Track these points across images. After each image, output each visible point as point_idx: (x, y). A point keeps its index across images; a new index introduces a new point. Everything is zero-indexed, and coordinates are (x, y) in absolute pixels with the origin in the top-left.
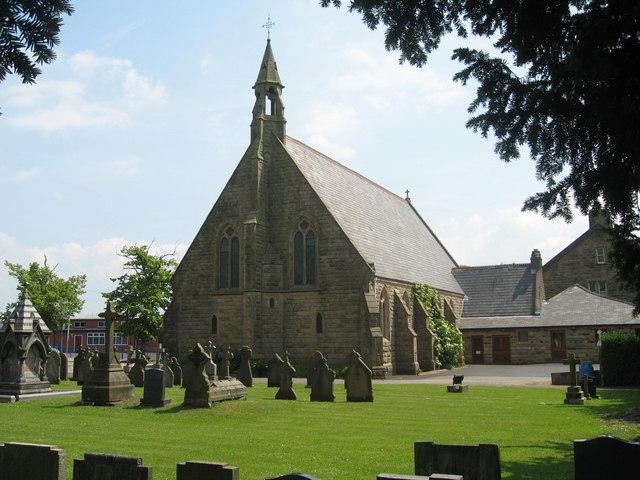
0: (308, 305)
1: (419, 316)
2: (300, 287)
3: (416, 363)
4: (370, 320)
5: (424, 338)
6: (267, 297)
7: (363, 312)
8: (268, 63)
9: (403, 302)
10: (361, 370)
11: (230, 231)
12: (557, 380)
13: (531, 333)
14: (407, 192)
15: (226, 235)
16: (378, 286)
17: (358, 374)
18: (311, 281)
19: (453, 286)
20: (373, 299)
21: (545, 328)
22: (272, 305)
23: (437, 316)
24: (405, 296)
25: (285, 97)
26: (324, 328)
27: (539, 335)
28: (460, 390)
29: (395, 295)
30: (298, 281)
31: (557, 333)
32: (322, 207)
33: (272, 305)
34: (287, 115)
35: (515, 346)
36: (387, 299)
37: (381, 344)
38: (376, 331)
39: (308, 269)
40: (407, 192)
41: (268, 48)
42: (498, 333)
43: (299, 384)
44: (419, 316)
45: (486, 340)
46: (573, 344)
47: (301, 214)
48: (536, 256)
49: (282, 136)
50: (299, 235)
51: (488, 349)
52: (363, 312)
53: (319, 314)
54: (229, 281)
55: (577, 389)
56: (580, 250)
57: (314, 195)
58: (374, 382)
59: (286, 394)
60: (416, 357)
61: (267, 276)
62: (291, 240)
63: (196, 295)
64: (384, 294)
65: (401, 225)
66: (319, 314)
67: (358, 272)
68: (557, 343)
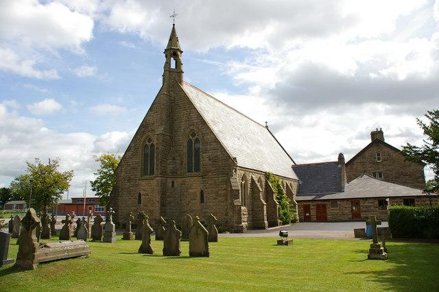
0: (195, 185)
1: (268, 192)
2: (190, 174)
3: (266, 222)
4: (235, 194)
5: (271, 206)
6: (169, 181)
7: (229, 189)
8: (173, 38)
9: (258, 184)
10: (200, 232)
11: (150, 140)
12: (359, 234)
13: (339, 203)
14: (266, 122)
15: (147, 143)
16: (240, 173)
17: (197, 234)
18: (197, 170)
19: (293, 175)
20: (236, 180)
21: (348, 199)
22: (173, 186)
23: (280, 192)
24: (259, 180)
25: (182, 58)
26: (205, 199)
27: (344, 204)
28: (287, 244)
29: (252, 178)
30: (190, 171)
31: (355, 201)
32: (204, 123)
33: (173, 186)
34: (184, 68)
35: (330, 211)
36: (246, 181)
37: (240, 210)
38: (238, 202)
39: (195, 163)
40: (266, 122)
41: (174, 28)
42: (320, 203)
43: (157, 246)
44: (268, 192)
45: (312, 207)
46: (365, 209)
47: (191, 127)
48: (341, 157)
49: (181, 81)
50: (190, 142)
51: (313, 213)
52: (229, 189)
53: (202, 191)
54: (148, 170)
55: (379, 246)
56: (367, 154)
57: (199, 116)
58: (209, 243)
59: (146, 250)
60: (266, 218)
61: (170, 167)
62: (185, 144)
63: (129, 180)
64: (244, 178)
65: (260, 139)
66: (202, 191)
67: (227, 163)
68: (355, 209)
